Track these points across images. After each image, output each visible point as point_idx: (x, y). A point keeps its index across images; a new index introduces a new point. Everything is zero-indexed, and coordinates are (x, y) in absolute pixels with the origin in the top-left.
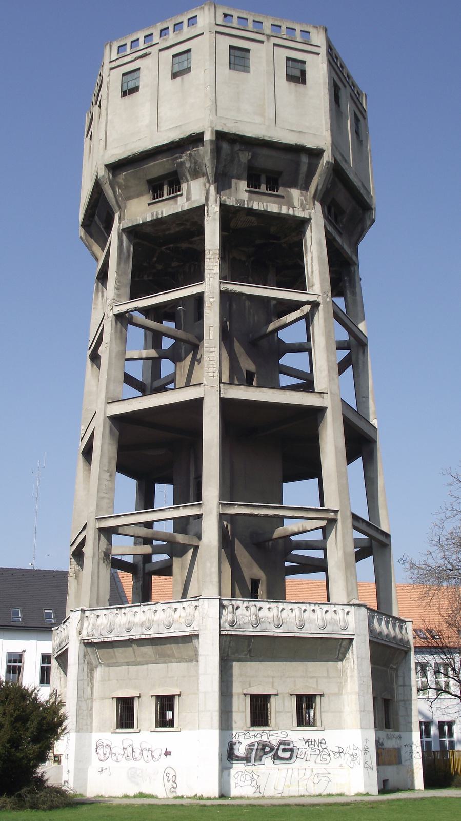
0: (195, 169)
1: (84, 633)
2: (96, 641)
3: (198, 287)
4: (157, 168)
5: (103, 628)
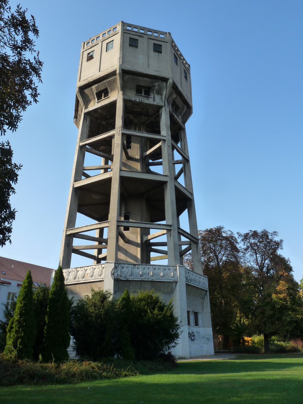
0: (159, 91)
1: (116, 275)
2: (122, 279)
3: (105, 135)
4: (144, 82)
5: (127, 273)
